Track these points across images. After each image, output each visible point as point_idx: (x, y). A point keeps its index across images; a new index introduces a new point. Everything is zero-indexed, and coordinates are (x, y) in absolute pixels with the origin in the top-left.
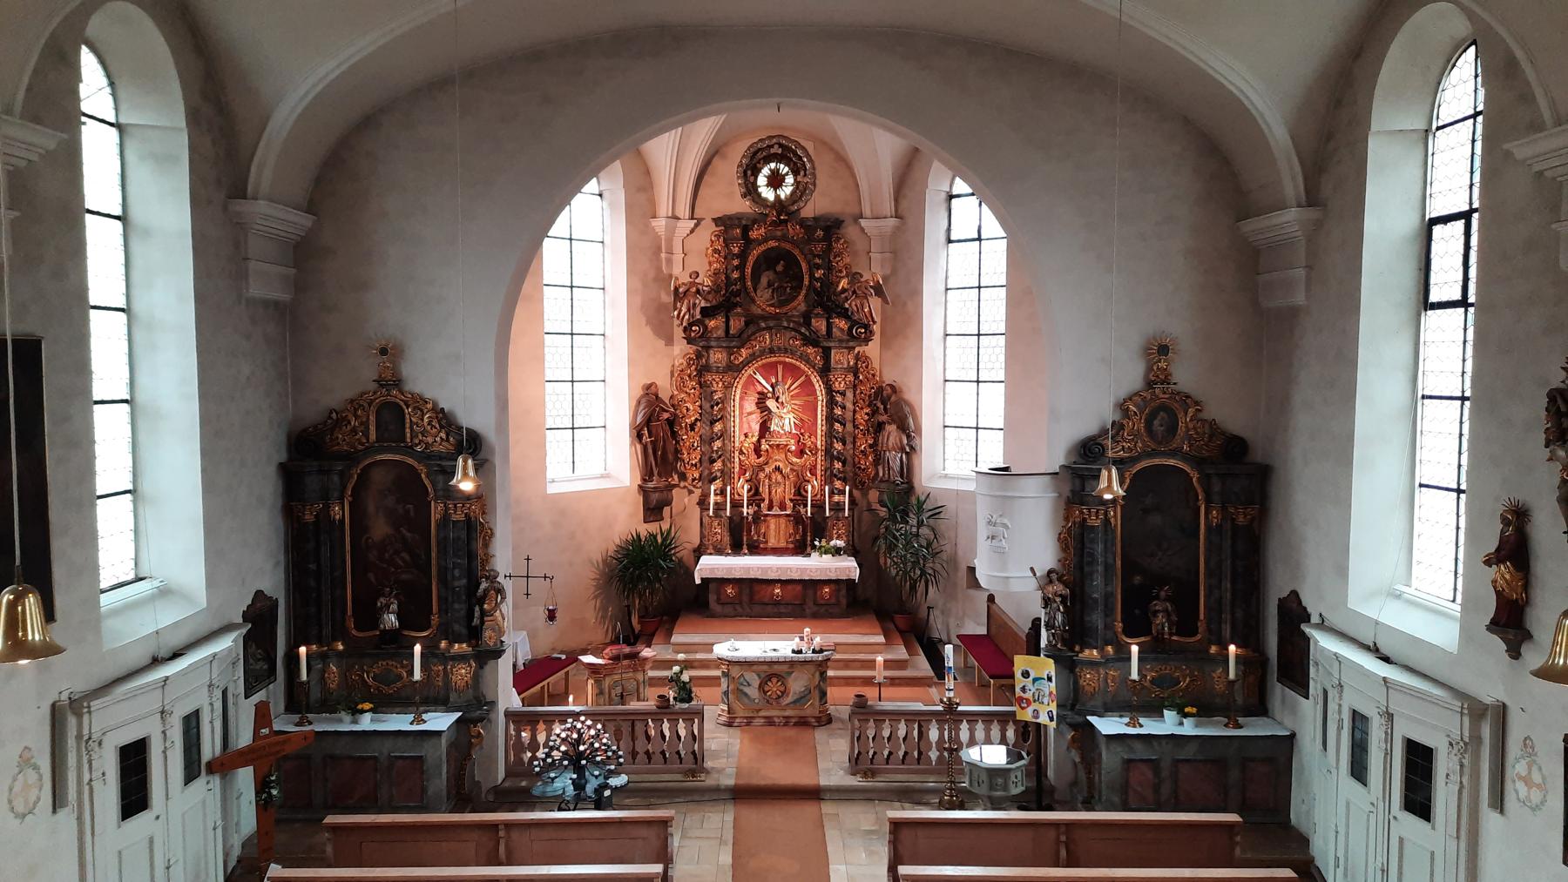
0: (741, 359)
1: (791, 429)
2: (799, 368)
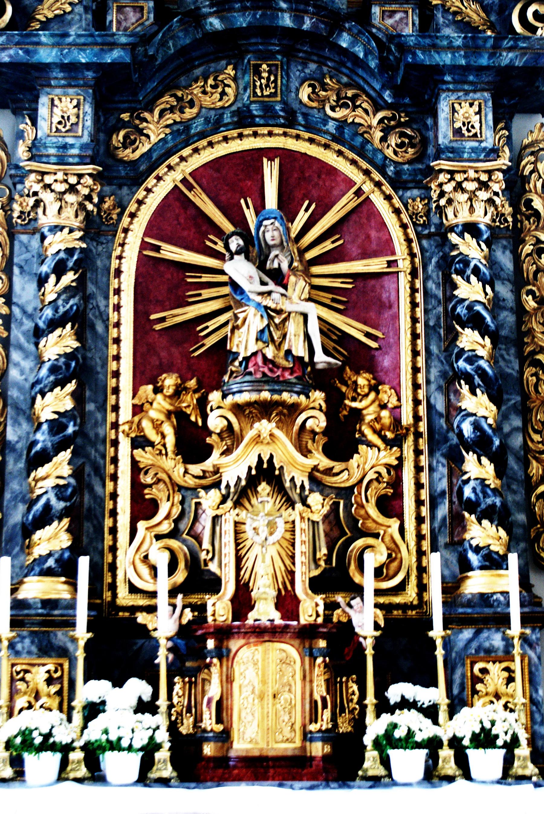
0: (145, 148)
1: (312, 352)
2: (332, 171)
